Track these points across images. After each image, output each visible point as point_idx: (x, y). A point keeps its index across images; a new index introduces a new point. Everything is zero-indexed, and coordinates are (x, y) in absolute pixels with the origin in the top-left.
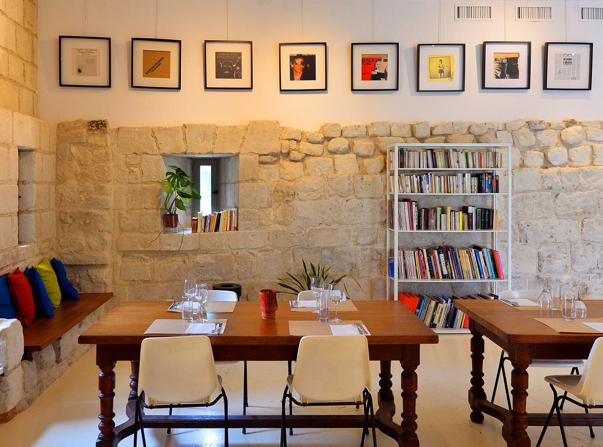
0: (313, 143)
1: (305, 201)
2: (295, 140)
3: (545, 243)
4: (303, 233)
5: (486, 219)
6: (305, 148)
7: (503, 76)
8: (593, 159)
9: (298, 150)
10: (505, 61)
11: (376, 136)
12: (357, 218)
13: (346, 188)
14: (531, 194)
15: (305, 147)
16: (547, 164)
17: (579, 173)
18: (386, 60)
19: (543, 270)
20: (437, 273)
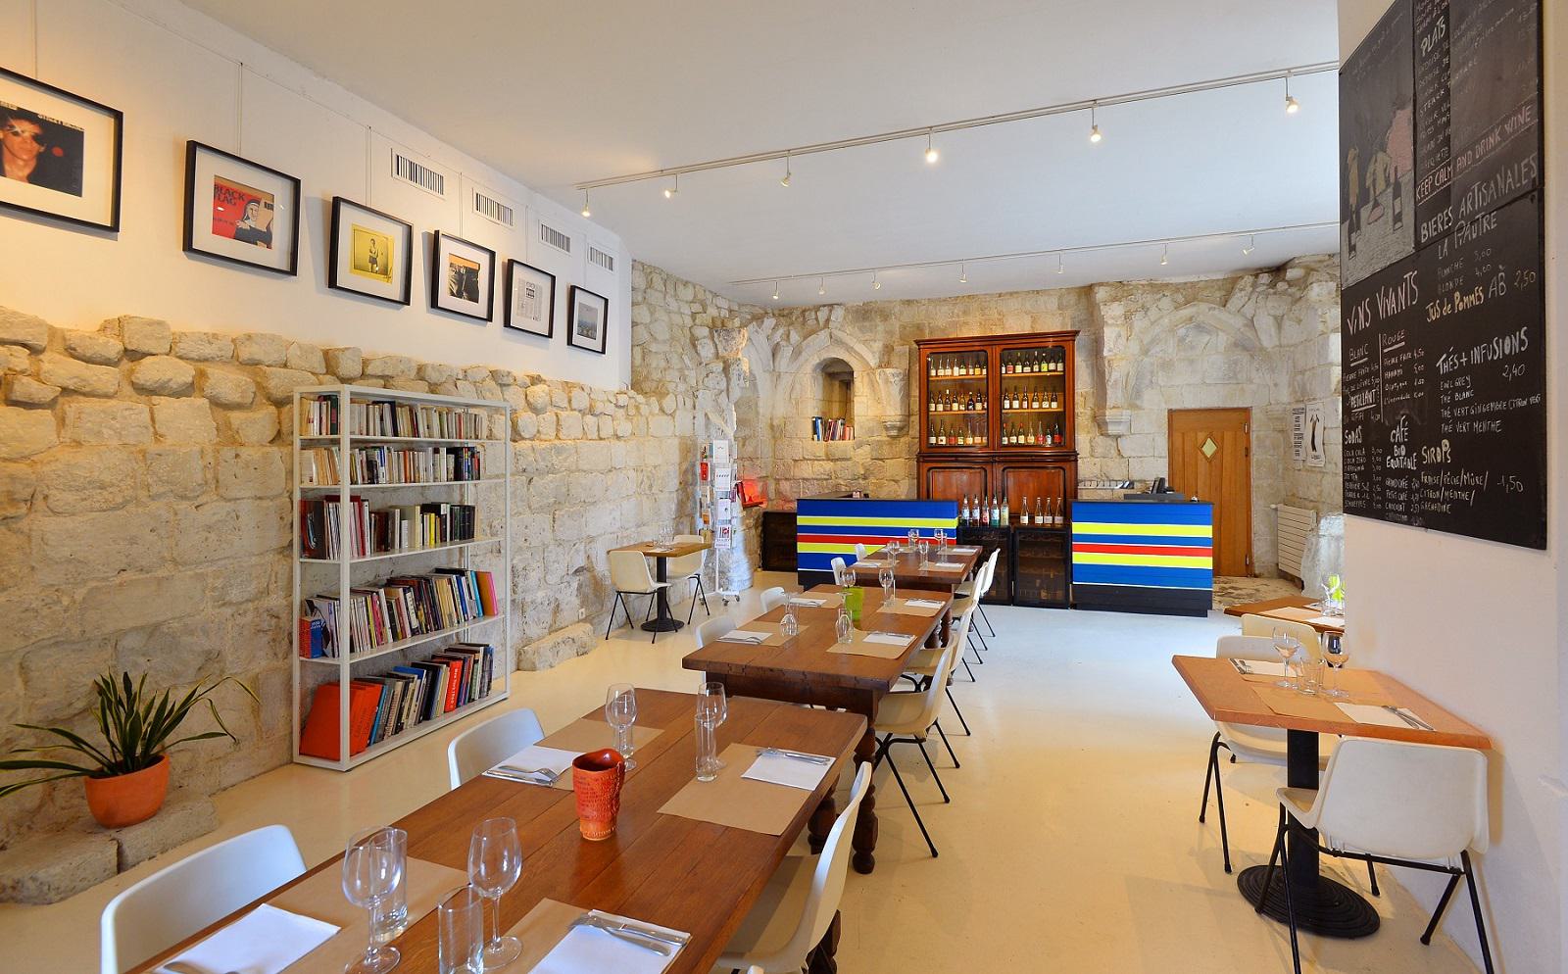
0: (88, 360)
1: (74, 514)
2: (24, 345)
4: (66, 601)
5: (462, 524)
6: (62, 372)
7: (459, 295)
8: (558, 430)
9: (37, 376)
11: (256, 363)
12: (224, 545)
13: (199, 477)
15: (60, 369)
16: (516, 435)
18: (270, 207)
19: (519, 590)
20: (403, 629)
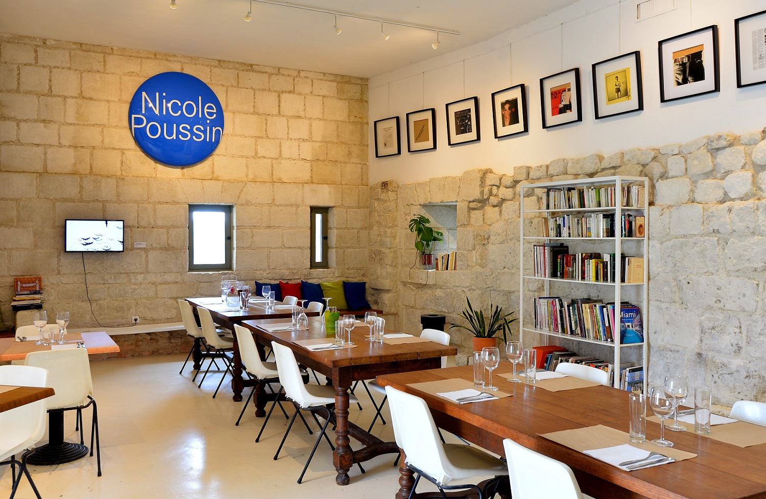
3: (710, 308)
7: (685, 81)
10: (686, 60)
14: (692, 240)
17: (757, 209)
